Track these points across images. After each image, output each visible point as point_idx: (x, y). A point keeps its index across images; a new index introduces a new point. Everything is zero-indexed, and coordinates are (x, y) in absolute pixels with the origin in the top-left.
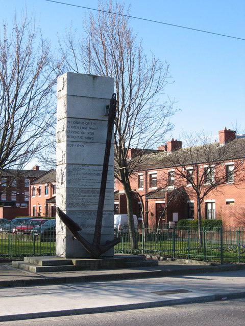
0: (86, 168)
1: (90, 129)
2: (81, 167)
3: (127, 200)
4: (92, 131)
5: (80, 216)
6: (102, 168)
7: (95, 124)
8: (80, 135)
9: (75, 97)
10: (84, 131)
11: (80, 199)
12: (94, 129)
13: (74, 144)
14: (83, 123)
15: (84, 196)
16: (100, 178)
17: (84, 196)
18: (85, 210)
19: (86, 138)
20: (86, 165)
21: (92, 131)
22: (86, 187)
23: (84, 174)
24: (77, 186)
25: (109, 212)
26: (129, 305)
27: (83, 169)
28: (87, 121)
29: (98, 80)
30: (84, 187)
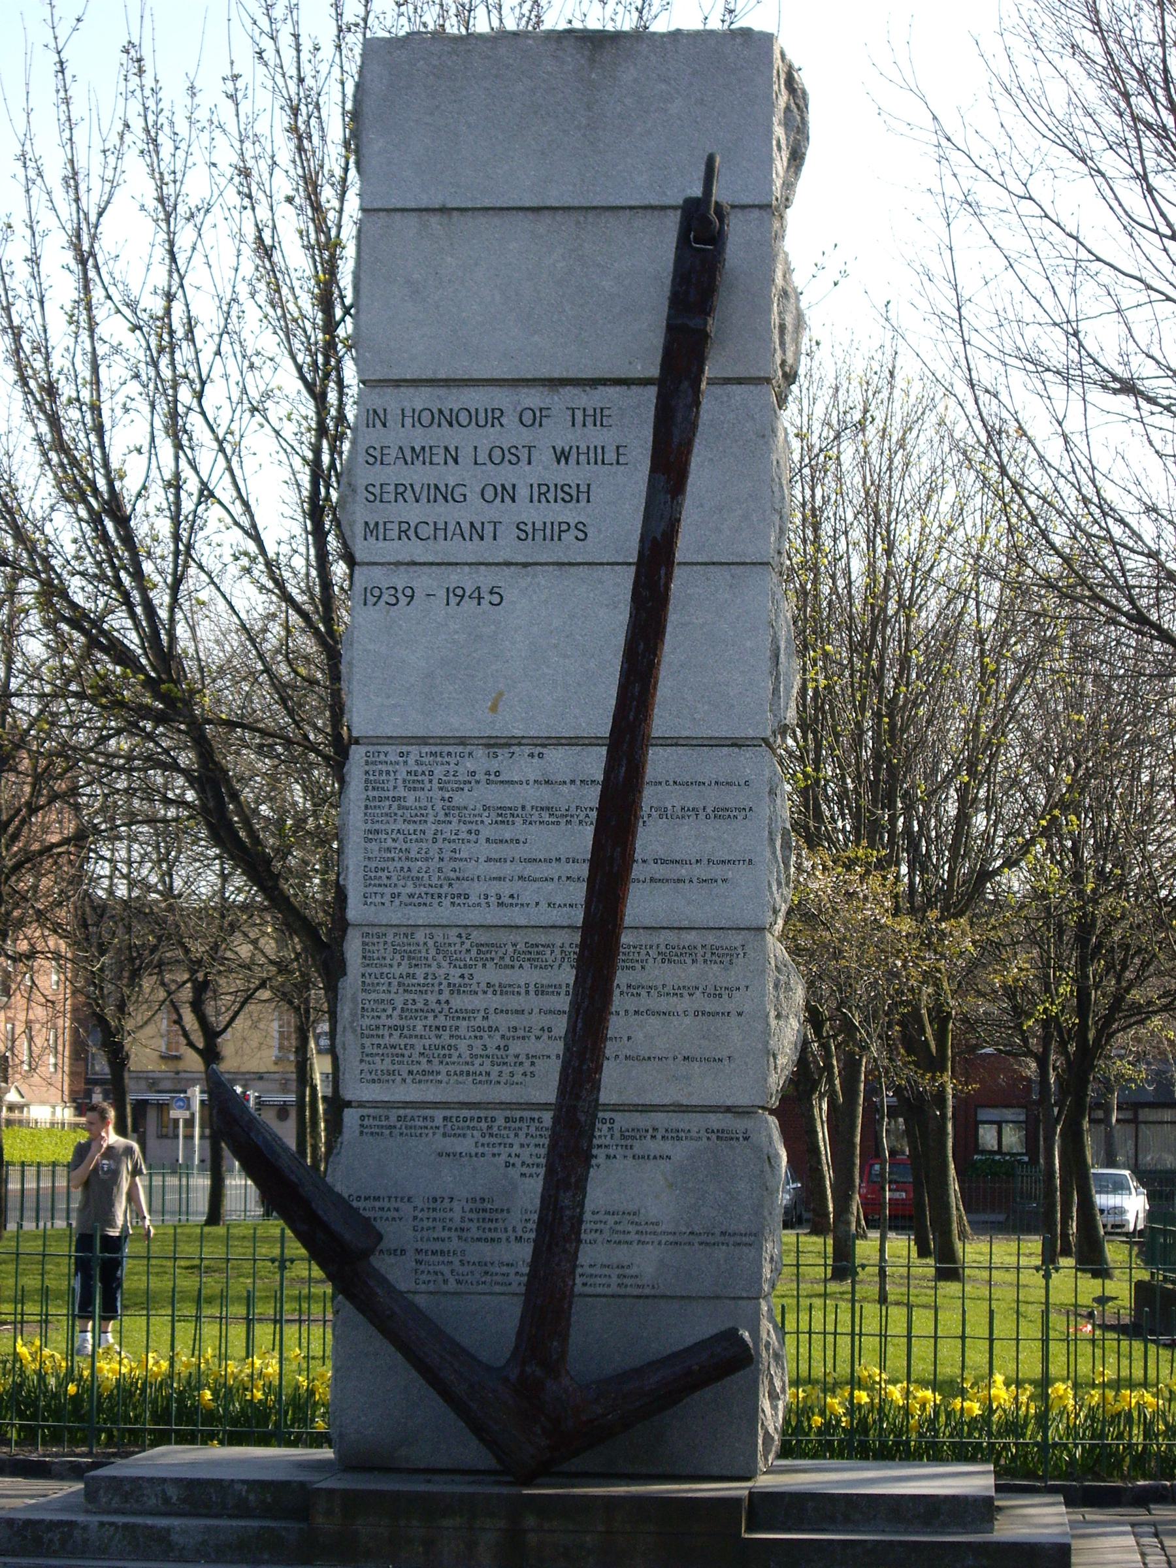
0: (522, 767)
1: (562, 456)
2: (479, 761)
3: (858, 1140)
4: (570, 474)
5: (465, 1145)
6: (594, 763)
7: (598, 417)
8: (473, 511)
9: (434, 219)
10: (505, 475)
11: (466, 1014)
12: (597, 456)
13: (423, 581)
14: (495, 417)
15: (503, 989)
16: (650, 839)
17: (503, 989)
18: (504, 1094)
19: (524, 532)
20: (519, 741)
21: (570, 474)
22: (518, 917)
23: (505, 815)
24: (444, 913)
25: (716, 1121)
26: (946, 1497)
27: (494, 778)
28: (533, 398)
29: (629, 74)
30: (493, 916)
